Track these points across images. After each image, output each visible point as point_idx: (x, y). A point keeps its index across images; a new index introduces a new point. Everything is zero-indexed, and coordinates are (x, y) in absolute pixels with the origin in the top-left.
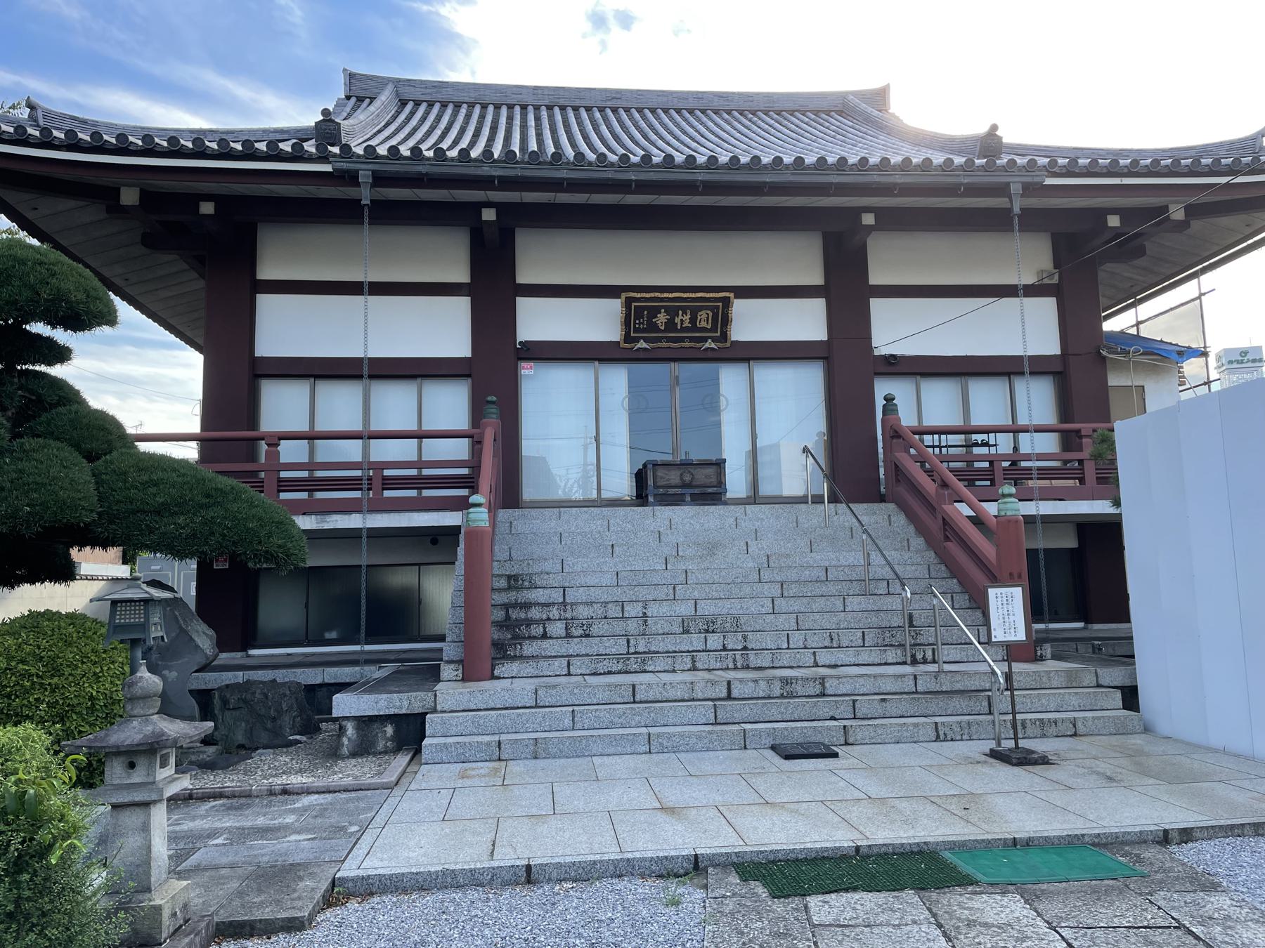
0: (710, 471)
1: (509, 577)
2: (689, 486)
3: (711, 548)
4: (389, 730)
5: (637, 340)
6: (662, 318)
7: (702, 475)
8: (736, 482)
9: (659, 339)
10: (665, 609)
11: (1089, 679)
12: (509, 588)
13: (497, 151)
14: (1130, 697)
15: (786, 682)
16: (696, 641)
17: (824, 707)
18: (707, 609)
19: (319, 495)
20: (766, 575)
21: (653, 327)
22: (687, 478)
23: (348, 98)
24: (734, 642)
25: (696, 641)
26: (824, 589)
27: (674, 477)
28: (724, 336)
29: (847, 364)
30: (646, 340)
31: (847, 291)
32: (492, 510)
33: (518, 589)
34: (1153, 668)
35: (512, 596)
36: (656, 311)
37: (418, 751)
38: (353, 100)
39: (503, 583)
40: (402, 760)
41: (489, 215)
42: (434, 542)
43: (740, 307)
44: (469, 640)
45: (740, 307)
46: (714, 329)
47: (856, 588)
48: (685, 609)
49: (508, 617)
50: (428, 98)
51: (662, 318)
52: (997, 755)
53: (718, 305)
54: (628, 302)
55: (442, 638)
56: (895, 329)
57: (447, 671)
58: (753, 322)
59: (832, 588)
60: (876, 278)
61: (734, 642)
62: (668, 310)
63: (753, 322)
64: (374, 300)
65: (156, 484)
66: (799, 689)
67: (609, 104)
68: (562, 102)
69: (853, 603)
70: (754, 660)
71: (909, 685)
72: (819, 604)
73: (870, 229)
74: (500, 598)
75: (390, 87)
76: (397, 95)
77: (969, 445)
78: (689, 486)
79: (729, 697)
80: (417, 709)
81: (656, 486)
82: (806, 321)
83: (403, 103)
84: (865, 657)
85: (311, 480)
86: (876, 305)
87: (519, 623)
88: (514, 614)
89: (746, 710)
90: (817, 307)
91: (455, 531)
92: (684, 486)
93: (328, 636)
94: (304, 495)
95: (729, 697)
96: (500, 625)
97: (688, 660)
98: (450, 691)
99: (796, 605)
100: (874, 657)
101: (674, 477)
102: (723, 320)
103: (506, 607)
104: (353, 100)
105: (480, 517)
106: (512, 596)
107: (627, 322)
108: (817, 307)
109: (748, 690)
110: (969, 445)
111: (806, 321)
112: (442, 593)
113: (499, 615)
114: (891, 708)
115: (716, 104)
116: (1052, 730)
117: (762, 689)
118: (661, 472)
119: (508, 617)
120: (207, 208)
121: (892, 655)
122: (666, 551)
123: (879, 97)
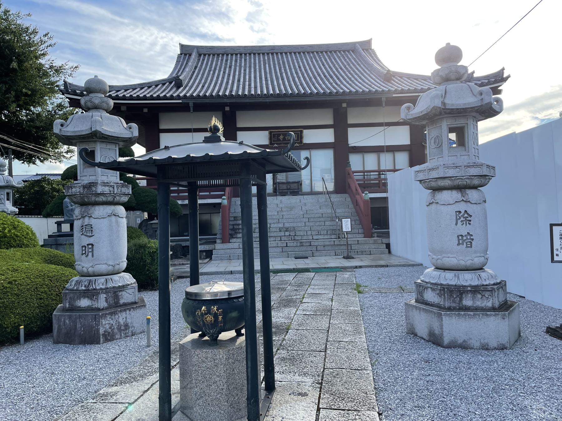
0: (296, 185)
1: (234, 217)
2: (289, 189)
3: (291, 208)
4: (204, 254)
5: (274, 144)
6: (281, 137)
7: (294, 186)
8: (305, 188)
9: (281, 144)
10: (276, 225)
11: (380, 242)
12: (234, 220)
13: (227, 93)
14: (388, 246)
15: (301, 243)
16: (282, 234)
17: (309, 248)
18: (287, 225)
19: (181, 194)
20: (305, 216)
21: (279, 140)
22: (289, 187)
23: (181, 54)
24: (292, 233)
25: (282, 234)
26: (320, 220)
27: (284, 187)
28: (301, 142)
29: (341, 150)
30: (277, 144)
31: (341, 127)
32: (229, 199)
33: (237, 220)
34: (394, 240)
35: (235, 222)
36: (279, 135)
37: (211, 259)
38: (183, 55)
39: (233, 219)
40: (208, 260)
41: (227, 109)
42: (215, 207)
43: (305, 132)
44: (223, 233)
45: (305, 132)
46: (298, 140)
47: (329, 219)
48: (281, 225)
49: (234, 228)
50: (208, 53)
51: (281, 137)
52: (344, 258)
53: (299, 131)
54: (270, 133)
55: (216, 235)
56: (356, 138)
57: (218, 241)
58: (310, 137)
59: (322, 219)
60: (350, 121)
61: (292, 233)
62: (283, 135)
63: (310, 137)
64: (194, 134)
65: (147, 196)
66: (304, 244)
67: (271, 51)
68: (254, 52)
69: (327, 223)
70: (296, 238)
71: (333, 243)
72: (317, 224)
73: (346, 108)
74: (231, 223)
75: (195, 50)
76: (198, 52)
77: (380, 174)
78: (289, 189)
79: (287, 246)
80: (211, 249)
81: (279, 190)
82: (327, 136)
83: (200, 55)
84: (326, 237)
85: (178, 190)
86: (350, 130)
87: (236, 229)
88: (235, 227)
89: (290, 249)
90: (331, 131)
91: (220, 204)
92: (288, 189)
93: (185, 234)
94: (176, 194)
95: (287, 246)
96: (231, 230)
97: (279, 238)
98: (219, 246)
99: (311, 224)
100: (328, 237)
101: (284, 187)
102: (300, 136)
103: (233, 225)
104: (183, 55)
105: (225, 202)
106: (235, 222)
107: (270, 139)
108: (331, 131)
109: (292, 244)
110: (380, 174)
111: (328, 136)
112: (217, 220)
113: (231, 227)
114: (326, 248)
115: (308, 50)
116: (365, 253)
117: (295, 244)
118: (281, 185)
119: (234, 228)
120: (146, 110)
121: (333, 236)
122: (278, 209)
123: (366, 45)
